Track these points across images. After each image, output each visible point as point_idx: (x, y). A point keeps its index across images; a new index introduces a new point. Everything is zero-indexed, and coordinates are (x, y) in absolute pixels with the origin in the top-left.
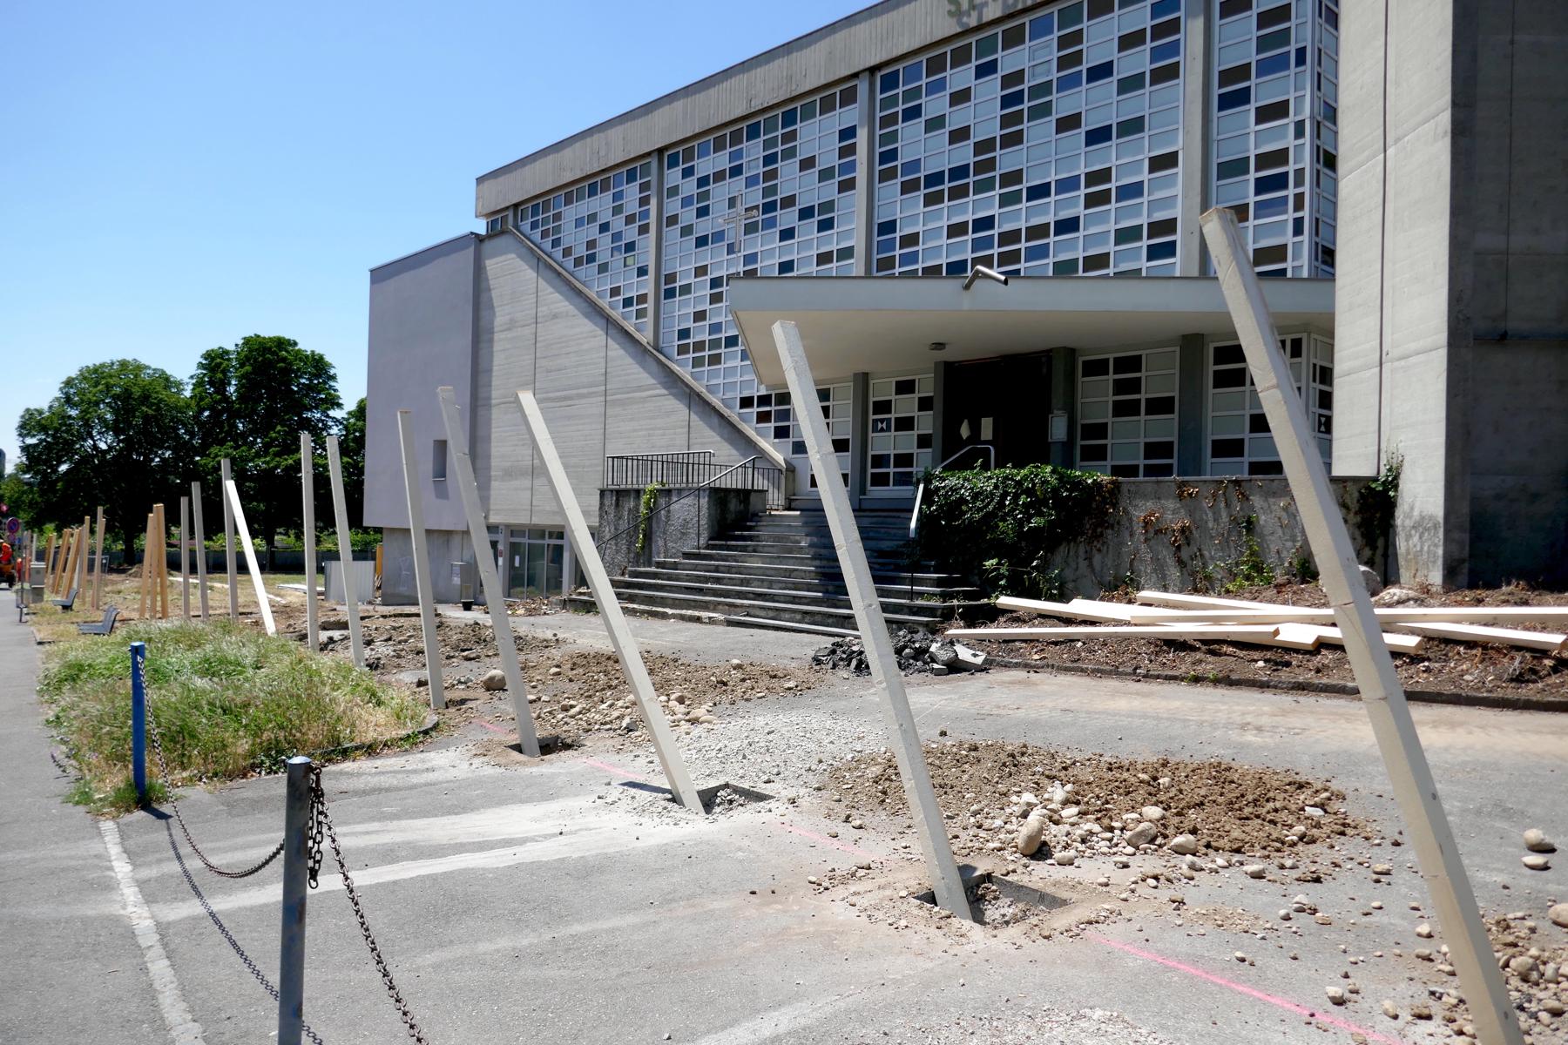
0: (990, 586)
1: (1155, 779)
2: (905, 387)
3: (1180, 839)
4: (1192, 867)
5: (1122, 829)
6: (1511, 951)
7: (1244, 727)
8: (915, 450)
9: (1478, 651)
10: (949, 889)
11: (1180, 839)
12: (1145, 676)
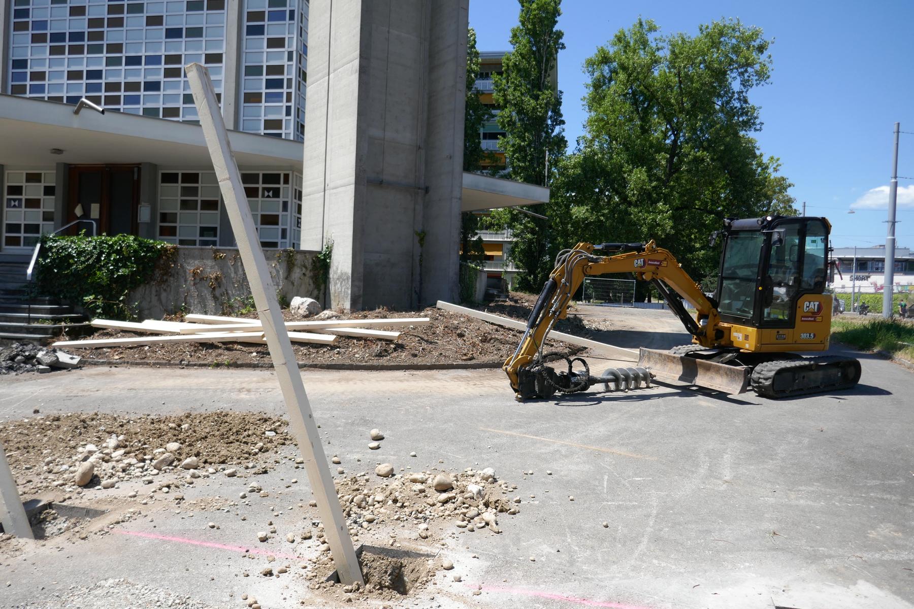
0: (91, 313)
1: (179, 426)
2: (33, 178)
3: (188, 460)
4: (194, 476)
5: (151, 460)
6: (355, 493)
7: (240, 390)
8: (41, 222)
9: (362, 342)
10: (14, 520)
11: (188, 460)
12: (187, 365)
